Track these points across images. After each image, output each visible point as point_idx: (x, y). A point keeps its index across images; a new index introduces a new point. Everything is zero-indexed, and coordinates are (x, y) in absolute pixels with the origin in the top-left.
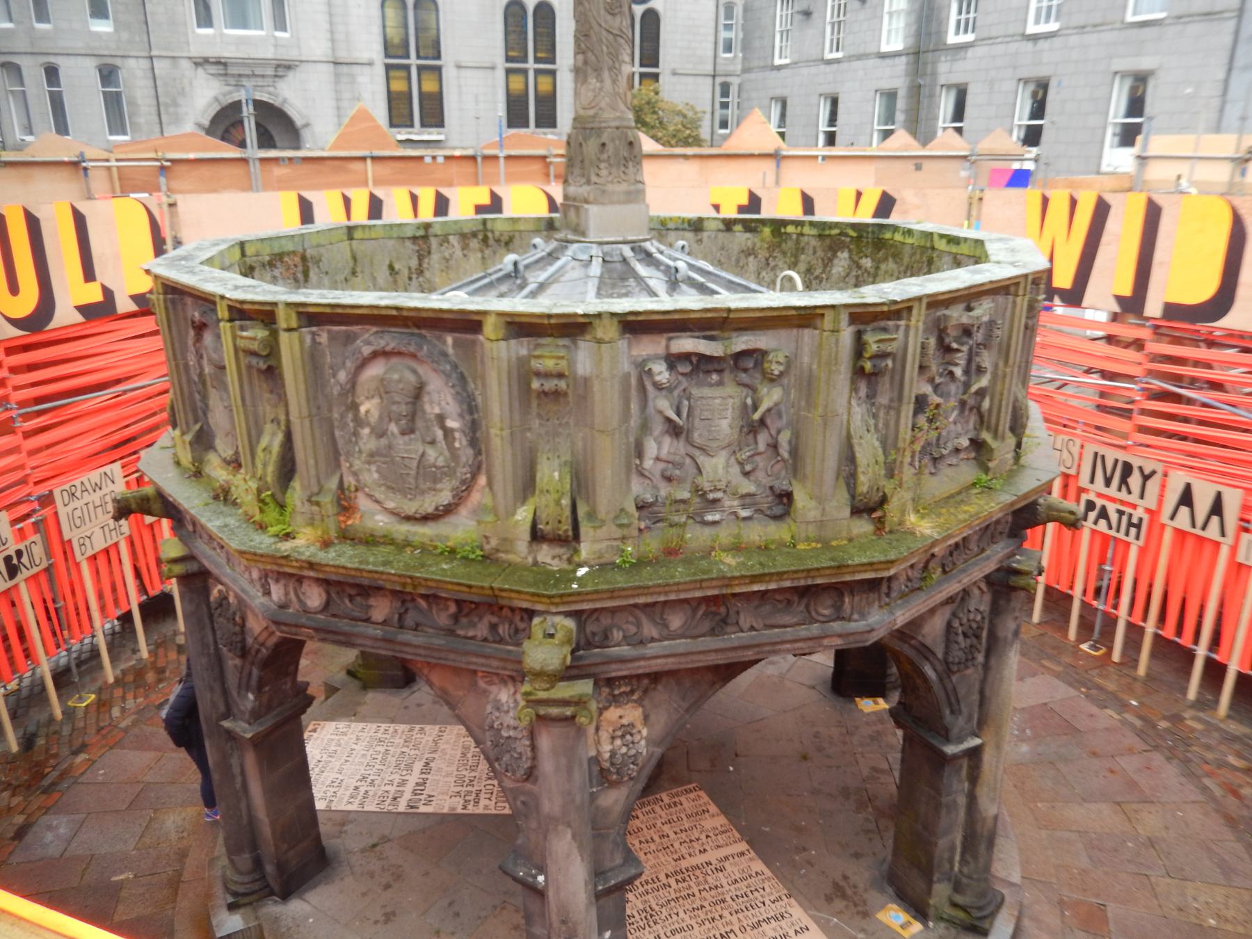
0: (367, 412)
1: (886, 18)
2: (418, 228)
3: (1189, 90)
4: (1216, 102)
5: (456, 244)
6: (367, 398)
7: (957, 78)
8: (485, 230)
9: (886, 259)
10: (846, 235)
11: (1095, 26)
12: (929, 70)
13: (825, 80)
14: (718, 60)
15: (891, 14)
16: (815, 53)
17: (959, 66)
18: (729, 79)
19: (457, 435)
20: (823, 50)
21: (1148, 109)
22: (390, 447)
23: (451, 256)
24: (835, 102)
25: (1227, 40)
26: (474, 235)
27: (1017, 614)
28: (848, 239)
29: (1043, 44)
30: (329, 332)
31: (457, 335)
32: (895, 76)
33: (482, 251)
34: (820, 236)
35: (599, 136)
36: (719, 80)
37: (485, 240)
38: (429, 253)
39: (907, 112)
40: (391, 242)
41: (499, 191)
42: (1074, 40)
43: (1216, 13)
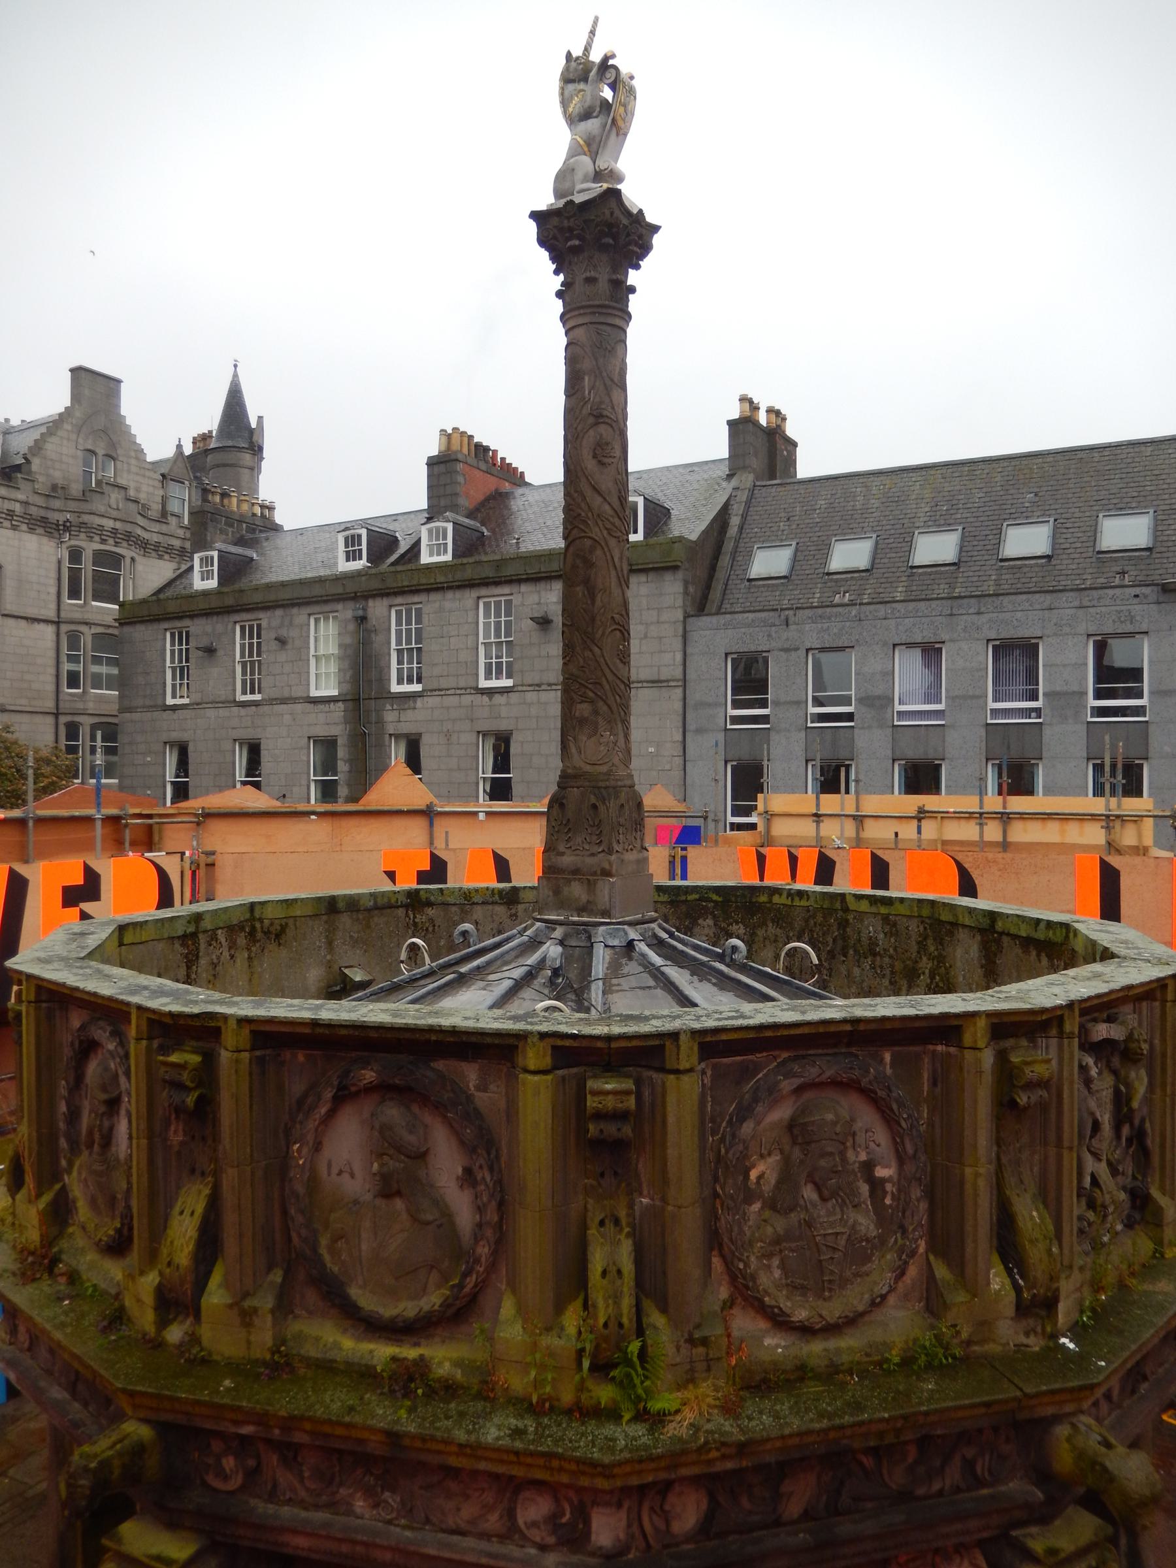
0: (760, 1177)
1: (313, 662)
2: (189, 922)
3: (651, 750)
4: (679, 761)
5: (223, 940)
6: (762, 1156)
7: (405, 728)
8: (253, 918)
9: (763, 924)
10: (710, 900)
11: (550, 685)
12: (373, 718)
13: (244, 725)
14: (61, 697)
15: (317, 658)
16: (223, 694)
17: (409, 715)
18: (77, 719)
19: (889, 1187)
20: (234, 690)
21: (514, 762)
22: (809, 1224)
23: (218, 958)
24: (183, 751)
25: (678, 706)
26: (241, 927)
27: (1115, 1290)
28: (711, 905)
29: (499, 699)
30: (715, 1067)
31: (897, 1048)
32: (333, 723)
33: (249, 949)
34: (671, 903)
35: (617, 797)
36: (63, 719)
37: (252, 933)
38: (197, 957)
39: (351, 761)
40: (160, 946)
41: (97, 865)
42: (531, 696)
43: (661, 681)
